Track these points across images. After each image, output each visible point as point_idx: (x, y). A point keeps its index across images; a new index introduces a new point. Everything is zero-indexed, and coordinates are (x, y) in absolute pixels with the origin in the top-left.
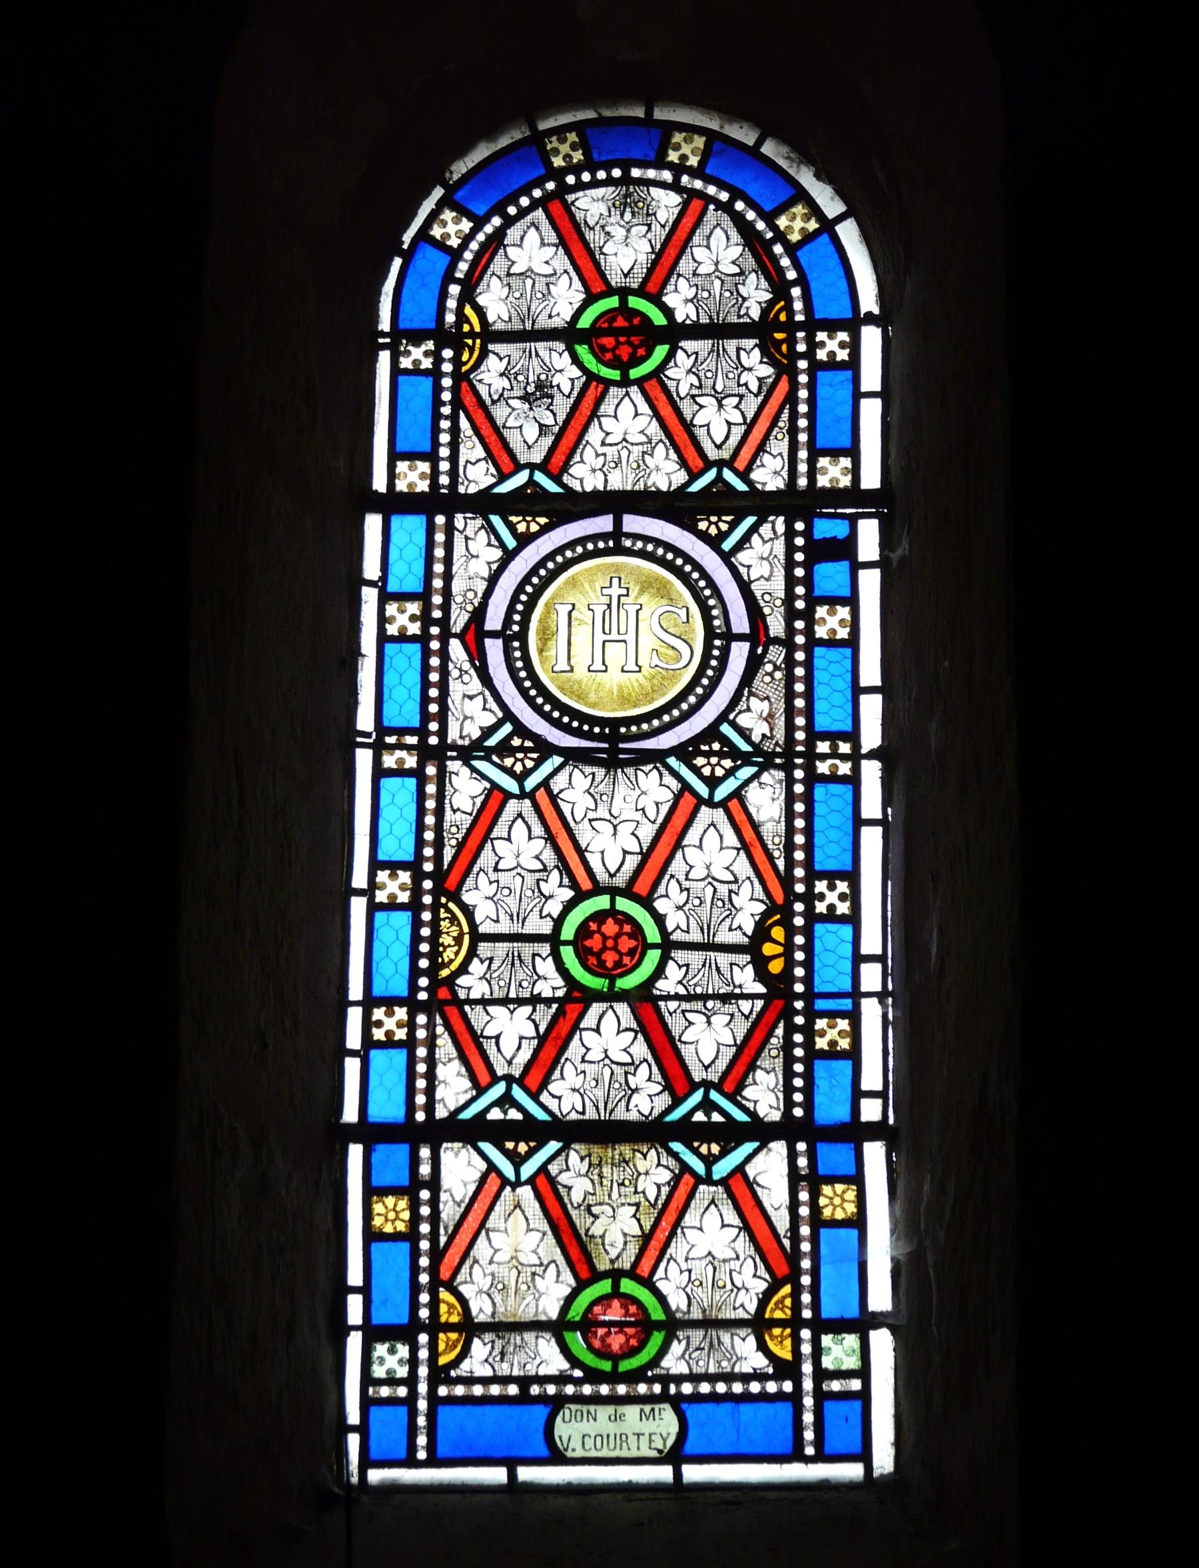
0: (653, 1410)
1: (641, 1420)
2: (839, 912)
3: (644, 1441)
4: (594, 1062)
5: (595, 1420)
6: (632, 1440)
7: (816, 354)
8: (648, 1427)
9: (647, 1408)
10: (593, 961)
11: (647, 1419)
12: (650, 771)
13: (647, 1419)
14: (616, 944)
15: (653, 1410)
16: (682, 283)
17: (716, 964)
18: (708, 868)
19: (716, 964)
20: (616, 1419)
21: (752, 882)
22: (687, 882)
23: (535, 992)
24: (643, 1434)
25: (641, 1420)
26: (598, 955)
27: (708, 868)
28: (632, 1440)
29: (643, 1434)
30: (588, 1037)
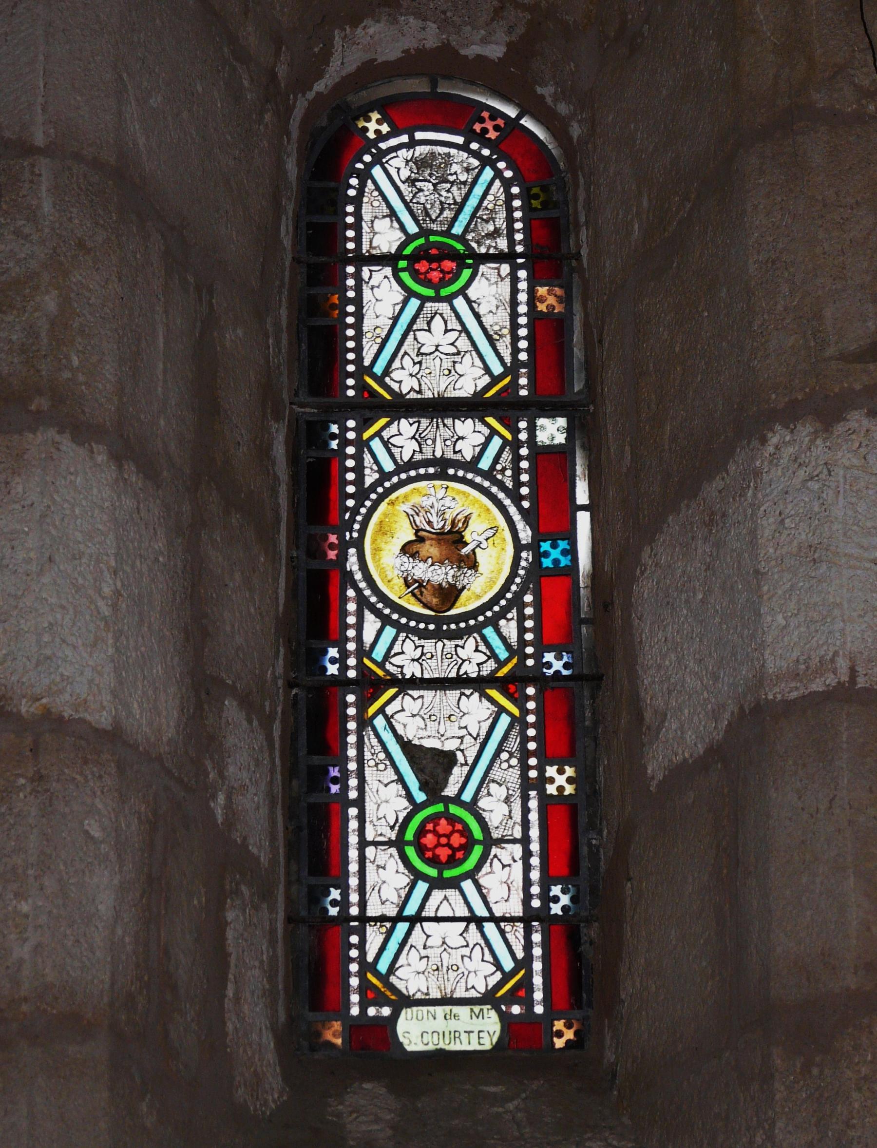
0: (482, 1010)
1: (471, 1018)
2: (384, 132)
3: (474, 1036)
4: (458, 704)
5: (435, 1018)
6: (464, 1037)
7: (389, 126)
8: (476, 1025)
9: (477, 1009)
10: (459, 855)
11: (478, 1017)
12: (409, 393)
13: (478, 1017)
14: (444, 835)
15: (482, 1010)
16: (407, 361)
17: (398, 738)
18: (419, 973)
19: (398, 738)
20: (451, 1019)
21: (389, 159)
22: (425, 951)
23: (412, 150)
24: (472, 1032)
25: (471, 1018)
26: (454, 850)
27: (419, 973)
28: (464, 1037)
29: (472, 1032)
30: (422, 336)
